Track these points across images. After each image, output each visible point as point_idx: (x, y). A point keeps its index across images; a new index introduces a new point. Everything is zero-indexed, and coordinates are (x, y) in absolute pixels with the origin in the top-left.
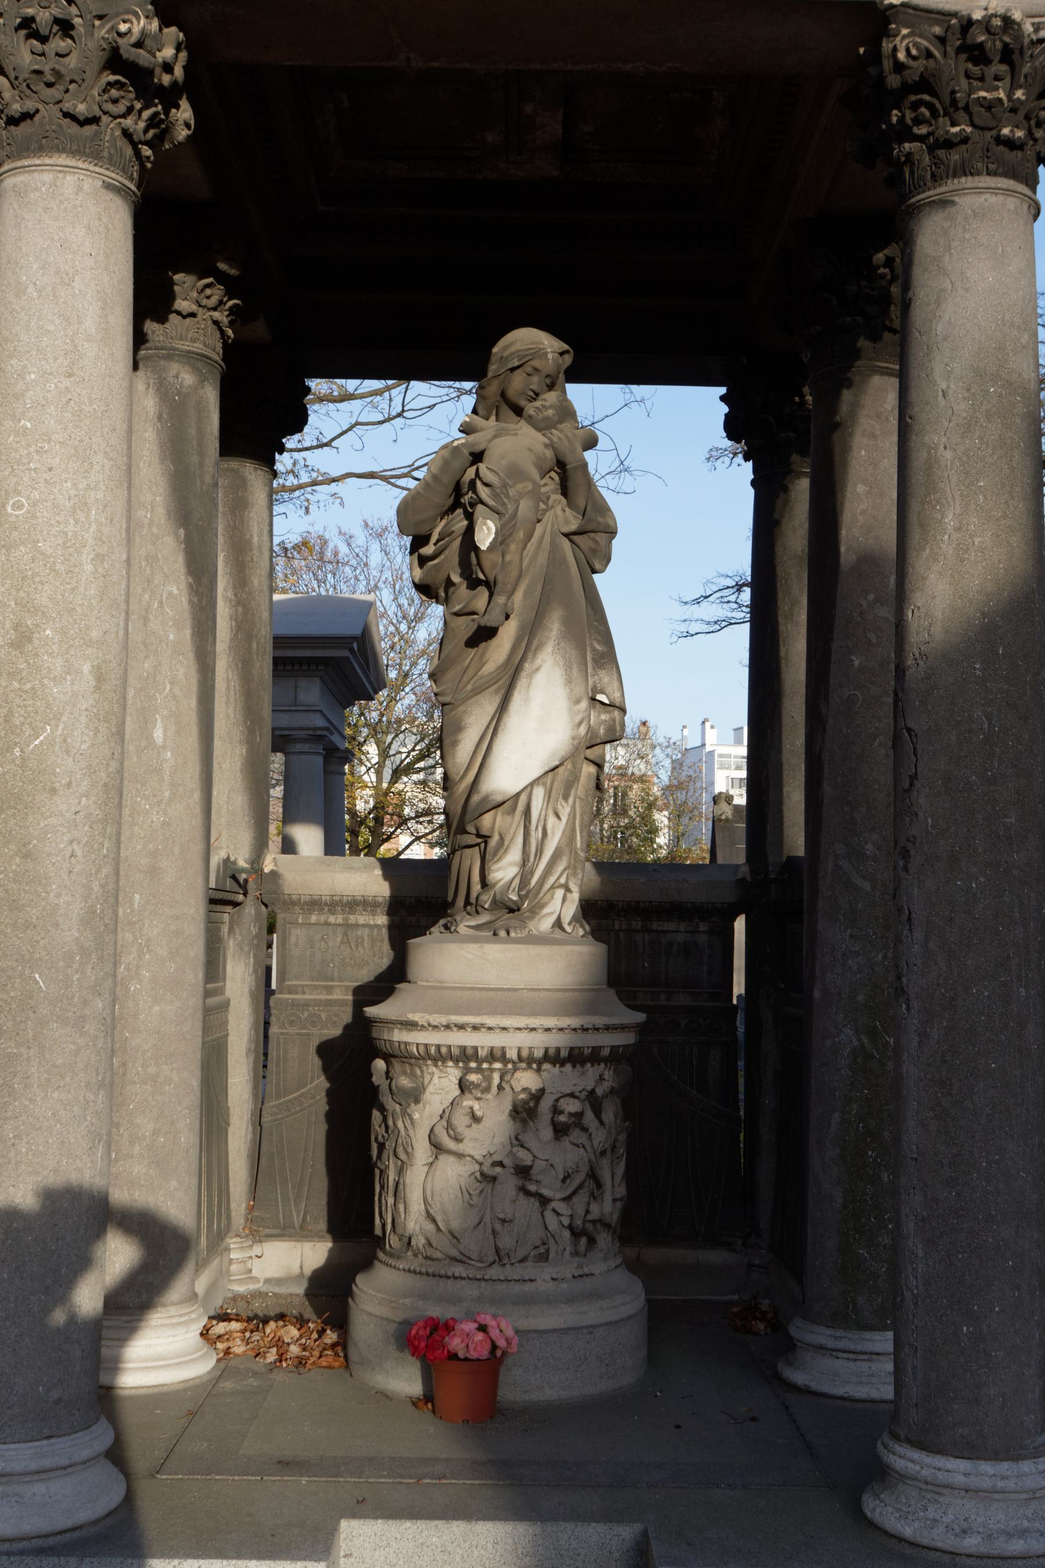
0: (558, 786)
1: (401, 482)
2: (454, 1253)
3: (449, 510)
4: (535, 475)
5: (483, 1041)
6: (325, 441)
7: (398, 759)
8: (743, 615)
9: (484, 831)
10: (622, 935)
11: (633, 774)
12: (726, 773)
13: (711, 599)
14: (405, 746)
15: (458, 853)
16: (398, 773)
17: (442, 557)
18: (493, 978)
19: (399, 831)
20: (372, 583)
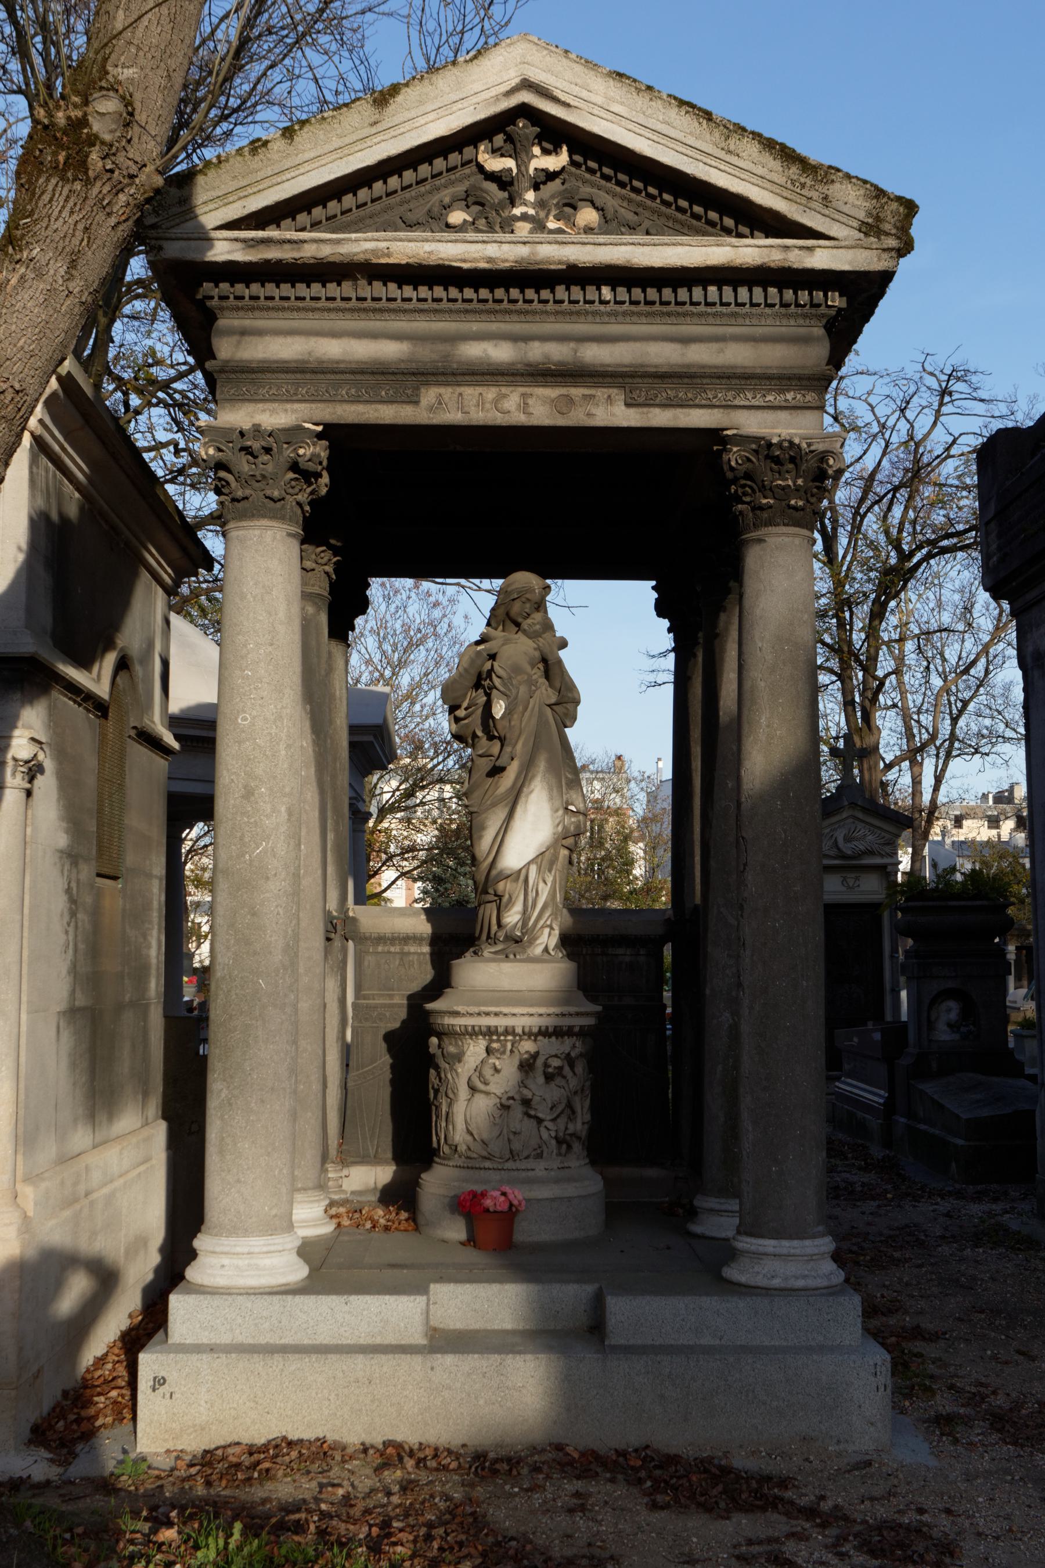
0: (545, 864)
2: (485, 1153)
4: (528, 668)
5: (501, 1022)
18: (506, 984)
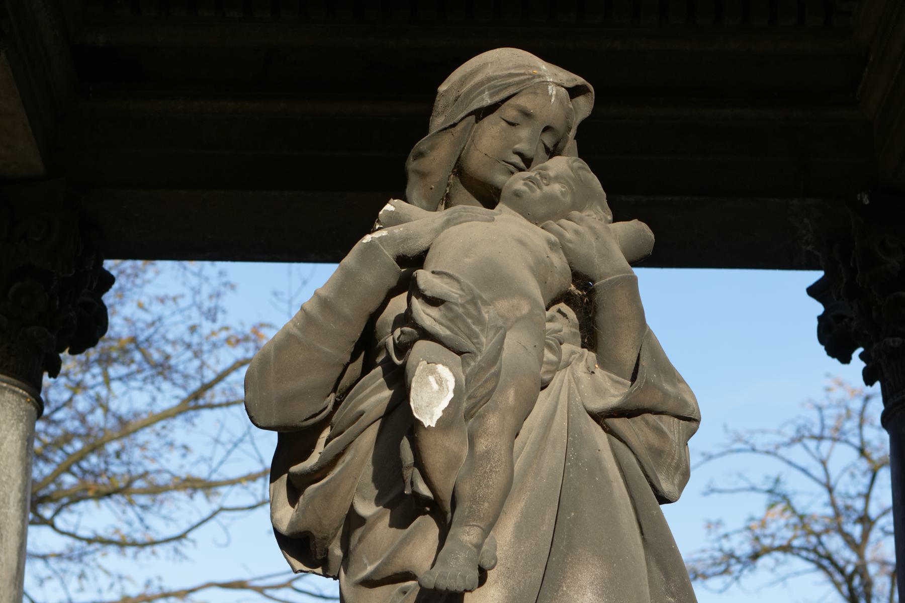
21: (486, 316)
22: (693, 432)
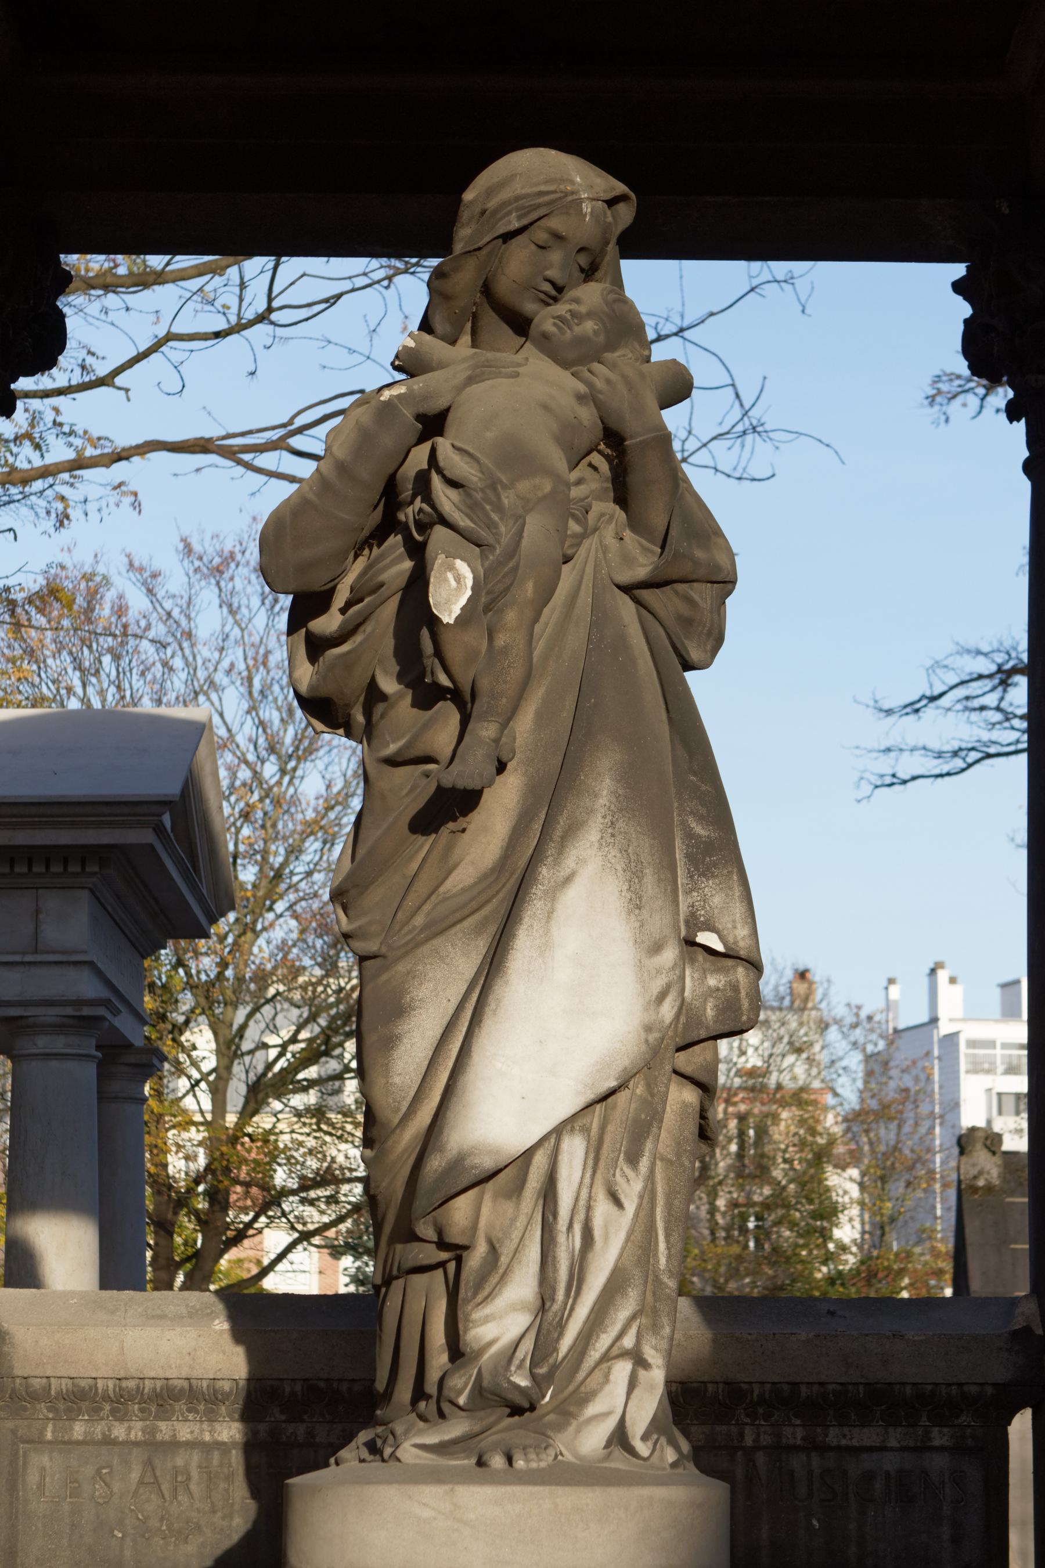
1: (267, 460)
3: (372, 536)
4: (558, 460)
6: (102, 369)
7: (259, 1061)
8: (1014, 735)
9: (455, 1236)
10: (760, 1458)
11: (779, 1087)
12: (984, 1081)
13: (945, 701)
14: (275, 1030)
15: (398, 1285)
16: (258, 1094)
17: (358, 638)
19: (263, 1219)
20: (201, 674)
21: (506, 501)
22: (729, 593)
